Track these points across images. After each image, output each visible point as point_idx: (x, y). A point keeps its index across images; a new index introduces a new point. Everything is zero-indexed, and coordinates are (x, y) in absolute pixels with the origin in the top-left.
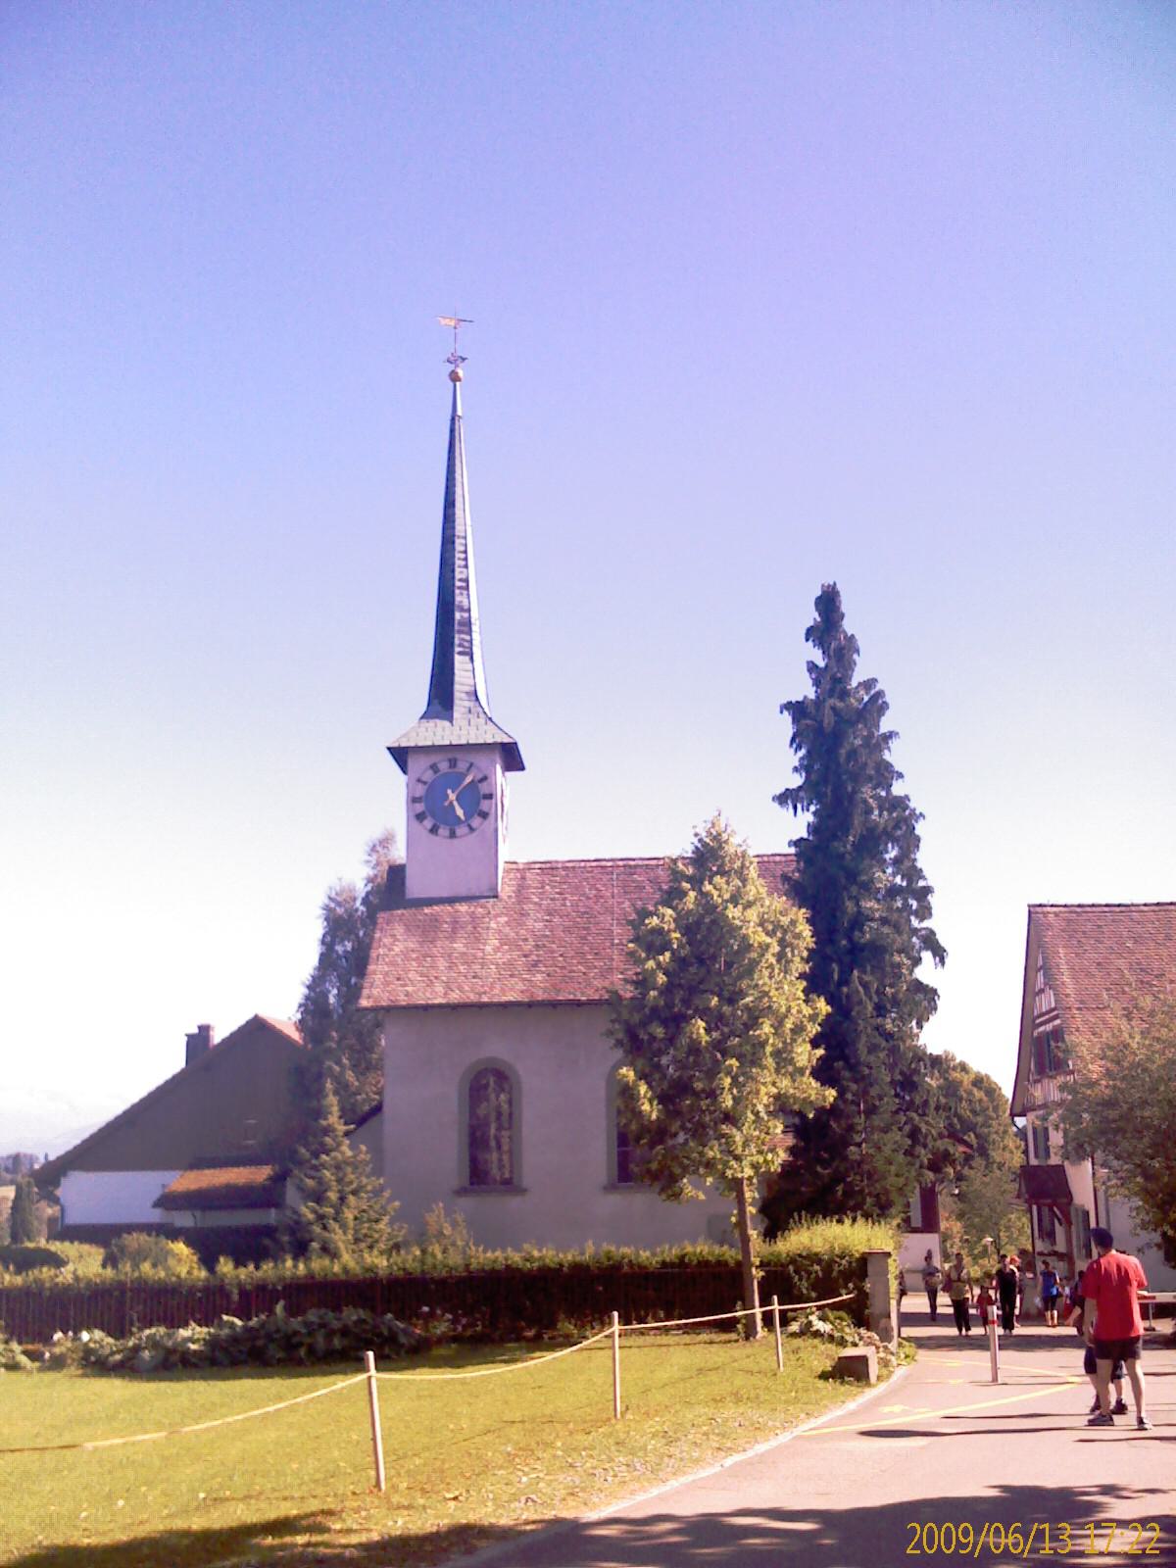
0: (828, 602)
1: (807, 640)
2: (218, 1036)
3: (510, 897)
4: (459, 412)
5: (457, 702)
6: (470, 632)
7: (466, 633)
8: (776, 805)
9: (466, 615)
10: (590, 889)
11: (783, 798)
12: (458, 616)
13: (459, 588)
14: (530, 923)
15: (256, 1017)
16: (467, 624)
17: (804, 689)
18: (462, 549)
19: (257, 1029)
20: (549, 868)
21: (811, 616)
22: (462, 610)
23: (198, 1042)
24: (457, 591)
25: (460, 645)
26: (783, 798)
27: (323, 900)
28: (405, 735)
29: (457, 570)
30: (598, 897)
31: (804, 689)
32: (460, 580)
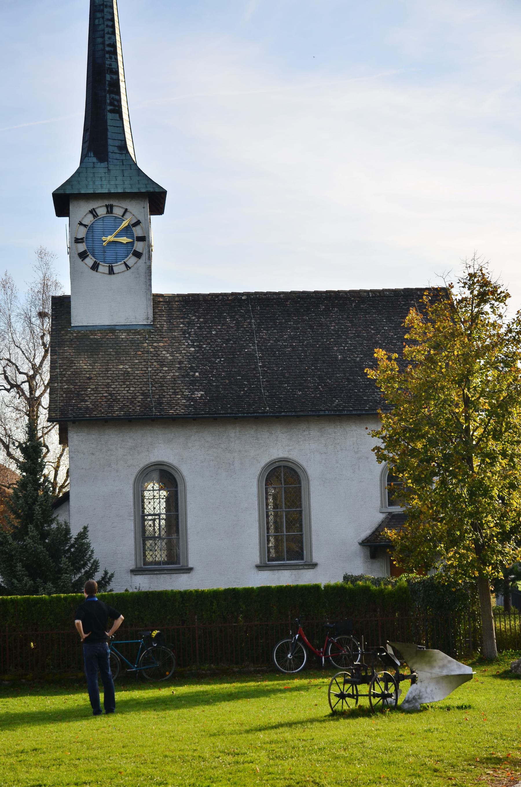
9: (115, 77)
24: (107, 56)
25: (111, 104)
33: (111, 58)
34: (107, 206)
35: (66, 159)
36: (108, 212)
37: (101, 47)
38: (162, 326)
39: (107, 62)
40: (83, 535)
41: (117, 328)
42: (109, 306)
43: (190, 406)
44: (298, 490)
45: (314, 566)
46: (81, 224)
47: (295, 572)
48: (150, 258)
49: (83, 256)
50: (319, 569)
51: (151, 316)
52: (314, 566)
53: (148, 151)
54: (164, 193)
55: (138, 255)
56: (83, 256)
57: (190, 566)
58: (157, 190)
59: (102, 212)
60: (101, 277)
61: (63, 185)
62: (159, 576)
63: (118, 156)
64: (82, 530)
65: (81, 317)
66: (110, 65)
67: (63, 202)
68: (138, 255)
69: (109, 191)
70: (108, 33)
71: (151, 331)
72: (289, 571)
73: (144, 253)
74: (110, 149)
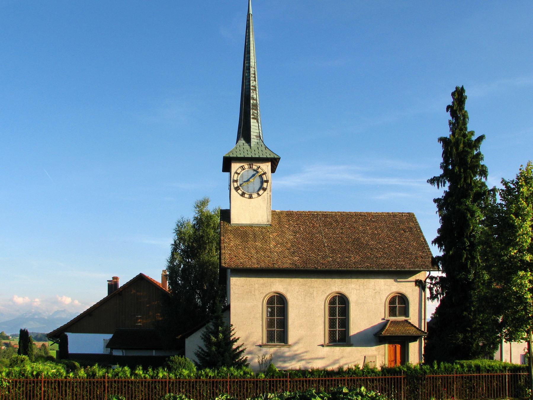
0: (459, 96)
1: (447, 111)
2: (121, 283)
3: (276, 225)
4: (251, 12)
5: (252, 140)
6: (256, 109)
7: (255, 110)
8: (429, 184)
9: (255, 102)
10: (310, 223)
11: (433, 181)
12: (252, 102)
13: (253, 89)
14: (287, 236)
15: (141, 274)
16: (256, 106)
17: (447, 133)
18: (253, 73)
19: (141, 280)
20: (290, 214)
21: (450, 101)
22: (253, 99)
23: (113, 286)
24: (251, 91)
25: (253, 115)
26: (433, 181)
27: (174, 226)
28: (231, 152)
29: (251, 82)
30: (314, 227)
31: (447, 133)
32: (253, 86)
51: (270, 220)
55: (265, 190)
58: (276, 157)
63: (256, 141)
65: (236, 219)
74: (252, 137)
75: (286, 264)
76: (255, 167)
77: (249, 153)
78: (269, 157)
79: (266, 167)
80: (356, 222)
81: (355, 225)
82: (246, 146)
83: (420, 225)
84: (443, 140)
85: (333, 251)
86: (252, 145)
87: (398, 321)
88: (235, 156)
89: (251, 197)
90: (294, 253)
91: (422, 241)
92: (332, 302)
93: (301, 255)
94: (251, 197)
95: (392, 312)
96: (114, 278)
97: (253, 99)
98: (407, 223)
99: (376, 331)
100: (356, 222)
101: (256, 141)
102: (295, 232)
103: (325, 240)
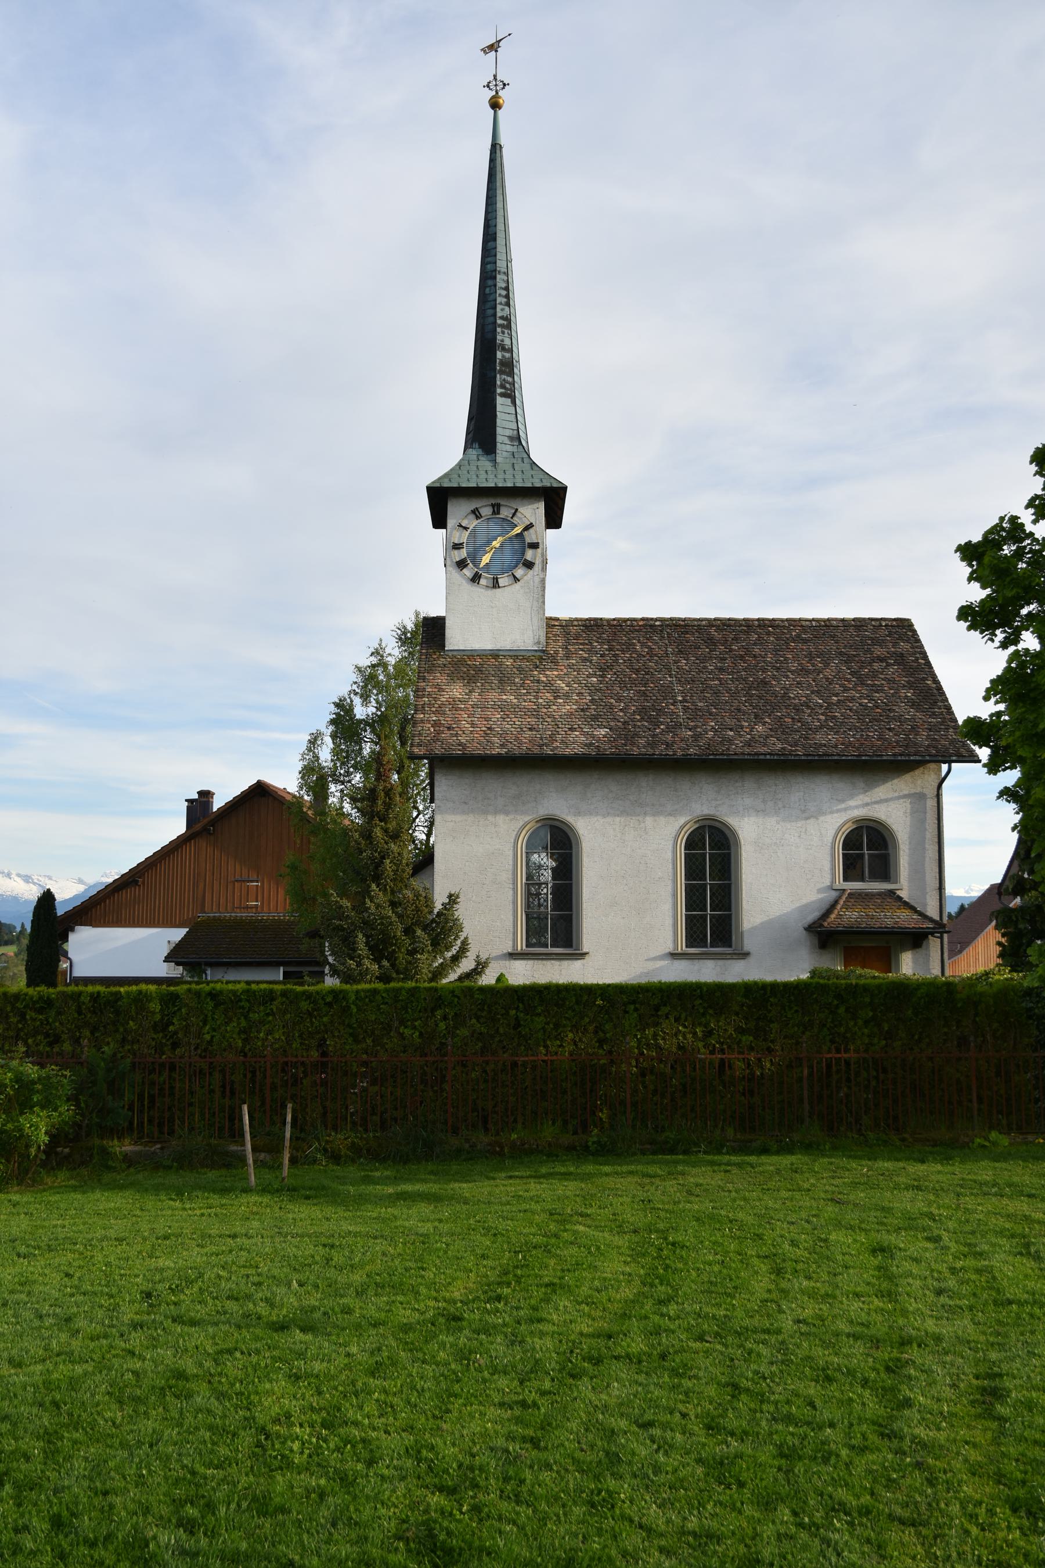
9: (507, 355)
12: (499, 355)
15: (259, 782)
18: (504, 285)
22: (504, 349)
24: (499, 330)
25: (502, 386)
29: (499, 307)
32: (502, 318)
33: (503, 333)
34: (493, 506)
35: (445, 450)
36: (494, 513)
37: (491, 319)
38: (556, 652)
39: (499, 337)
40: (453, 899)
41: (501, 653)
42: (490, 623)
43: (591, 744)
44: (728, 857)
45: (745, 955)
46: (460, 526)
47: (720, 962)
48: (544, 569)
49: (461, 564)
50: (751, 960)
51: (543, 639)
52: (745, 955)
53: (550, 434)
54: (564, 489)
55: (529, 565)
56: (461, 564)
57: (585, 950)
58: (555, 485)
59: (486, 512)
60: (480, 593)
61: (439, 479)
62: (545, 962)
63: (509, 448)
64: (447, 900)
65: (456, 639)
66: (502, 341)
67: (440, 499)
68: (529, 565)
69: (493, 498)
70: (501, 304)
71: (541, 658)
72: (712, 961)
73: (537, 562)
74: (499, 439)
75: (575, 743)
76: (505, 513)
77: (491, 476)
78: (538, 485)
79: (534, 512)
80: (760, 641)
81: (757, 650)
82: (485, 463)
83: (926, 648)
84: (969, 628)
85: (695, 714)
86: (499, 459)
87: (867, 894)
88: (456, 485)
89: (495, 584)
90: (595, 718)
91: (930, 688)
92: (693, 843)
93: (612, 724)
94: (495, 584)
95: (852, 868)
96: (200, 793)
97: (504, 349)
98: (892, 645)
99: (812, 917)
100: (760, 641)
101: (509, 448)
102: (603, 669)
103: (677, 688)
